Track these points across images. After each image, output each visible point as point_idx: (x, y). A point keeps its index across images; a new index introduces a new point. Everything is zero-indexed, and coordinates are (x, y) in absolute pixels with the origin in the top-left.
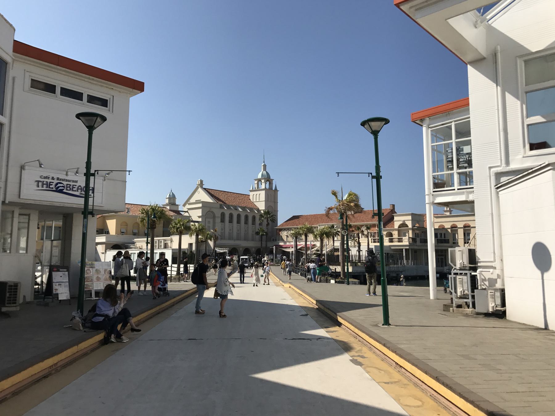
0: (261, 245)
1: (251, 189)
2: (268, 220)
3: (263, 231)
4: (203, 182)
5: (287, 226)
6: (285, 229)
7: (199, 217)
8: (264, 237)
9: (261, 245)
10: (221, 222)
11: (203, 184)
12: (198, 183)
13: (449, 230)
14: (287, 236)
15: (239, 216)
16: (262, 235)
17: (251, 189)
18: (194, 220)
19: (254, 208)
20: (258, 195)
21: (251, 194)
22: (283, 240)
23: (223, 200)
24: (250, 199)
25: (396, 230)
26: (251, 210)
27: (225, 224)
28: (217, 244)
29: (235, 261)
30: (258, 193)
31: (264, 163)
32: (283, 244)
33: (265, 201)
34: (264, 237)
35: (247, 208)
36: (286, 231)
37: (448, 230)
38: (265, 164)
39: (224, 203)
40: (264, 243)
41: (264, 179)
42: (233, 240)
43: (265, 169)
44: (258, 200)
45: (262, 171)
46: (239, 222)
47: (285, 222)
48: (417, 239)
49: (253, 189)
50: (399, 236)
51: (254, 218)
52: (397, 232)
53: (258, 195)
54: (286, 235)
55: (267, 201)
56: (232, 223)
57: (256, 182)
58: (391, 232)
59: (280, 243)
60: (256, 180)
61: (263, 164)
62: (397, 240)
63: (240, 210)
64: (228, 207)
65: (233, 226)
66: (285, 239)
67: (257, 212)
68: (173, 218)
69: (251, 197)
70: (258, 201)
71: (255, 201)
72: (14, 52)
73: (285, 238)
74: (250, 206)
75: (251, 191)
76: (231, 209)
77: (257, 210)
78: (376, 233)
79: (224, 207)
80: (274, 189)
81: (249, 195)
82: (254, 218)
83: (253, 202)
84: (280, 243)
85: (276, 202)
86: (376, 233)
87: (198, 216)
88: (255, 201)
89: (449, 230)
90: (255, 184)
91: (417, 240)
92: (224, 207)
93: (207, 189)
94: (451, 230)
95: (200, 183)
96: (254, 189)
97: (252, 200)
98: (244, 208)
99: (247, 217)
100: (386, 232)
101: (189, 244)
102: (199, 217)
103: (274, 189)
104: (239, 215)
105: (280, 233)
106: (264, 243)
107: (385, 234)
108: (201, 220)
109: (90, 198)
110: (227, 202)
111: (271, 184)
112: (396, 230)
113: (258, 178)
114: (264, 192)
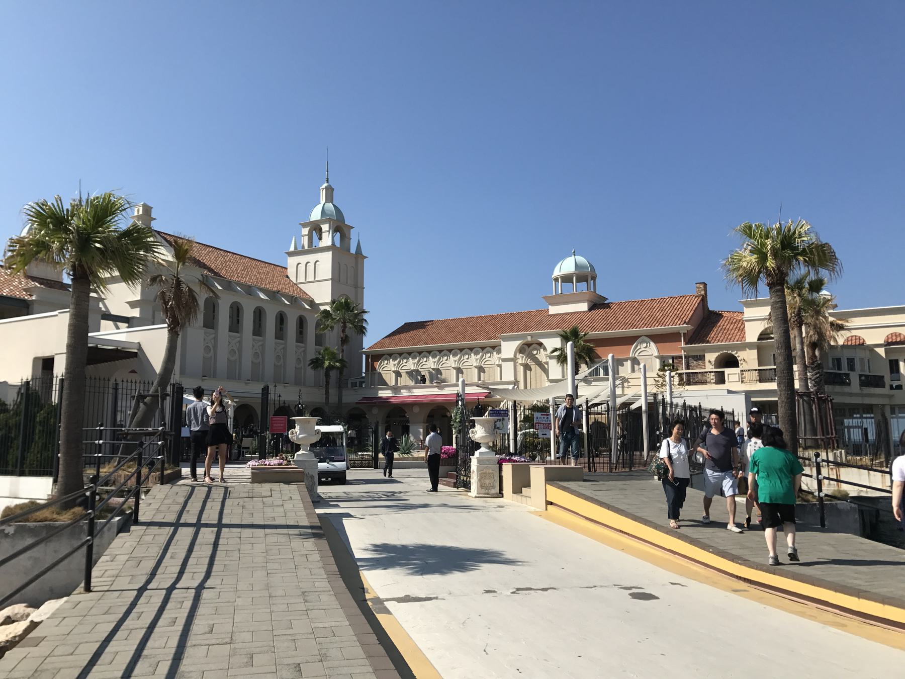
0: (327, 398)
1: (292, 249)
2: (345, 327)
3: (333, 357)
4: (153, 210)
5: (397, 346)
6: (390, 355)
7: (133, 305)
8: (333, 374)
9: (327, 398)
10: (204, 327)
11: (153, 216)
12: (136, 214)
13: (881, 351)
14: (398, 374)
15: (259, 314)
16: (330, 368)
17: (292, 249)
18: (113, 313)
19: (300, 298)
20: (311, 267)
21: (292, 262)
22: (383, 383)
23: (212, 266)
24: (287, 277)
25: (750, 346)
26: (294, 300)
27: (216, 333)
28: (244, 539)
29: (298, 447)
30: (311, 258)
31: (328, 183)
32: (391, 395)
33: (332, 279)
34: (333, 374)
35: (281, 294)
36: (394, 359)
37: (877, 350)
38: (330, 185)
39: (216, 274)
40: (333, 392)
41: (329, 221)
42: (239, 379)
43: (330, 198)
44: (310, 278)
45: (323, 201)
46: (258, 329)
47: (386, 337)
48: (851, 375)
49: (296, 248)
50: (759, 365)
51: (301, 322)
52: (755, 351)
53: (311, 267)
54: (394, 372)
55: (336, 280)
56: (237, 332)
57: (305, 231)
58: (734, 353)
59: (380, 392)
60: (304, 225)
61: (326, 185)
62: (755, 375)
63: (262, 296)
64: (229, 285)
65: (240, 342)
66: (392, 383)
67: (307, 307)
68: (34, 298)
69: (291, 272)
70: (313, 280)
71: (301, 279)
72: (100, 329)
73: (390, 379)
74: (290, 291)
75: (291, 254)
76: (236, 291)
77: (309, 302)
78: (681, 357)
79: (216, 284)
80: (353, 250)
81: (286, 269)
82: (301, 322)
83: (296, 284)
84: (380, 392)
85: (358, 286)
86: (681, 357)
87: (127, 303)
88: (301, 279)
89: (881, 351)
90: (303, 236)
91: (851, 377)
92: (216, 284)
93: (164, 233)
94: (886, 349)
95: (141, 213)
96: (300, 249)
97: (293, 279)
98: (274, 295)
99: (281, 319)
100: (715, 355)
101: (36, 360)
102: (133, 305)
103: (353, 250)
104: (260, 311)
105: (377, 365)
106: (333, 392)
107: (713, 360)
108: (138, 315)
109: (226, 445)
110: (223, 273)
111: (345, 237)
112: (750, 346)
113: (311, 220)
114: (329, 255)
